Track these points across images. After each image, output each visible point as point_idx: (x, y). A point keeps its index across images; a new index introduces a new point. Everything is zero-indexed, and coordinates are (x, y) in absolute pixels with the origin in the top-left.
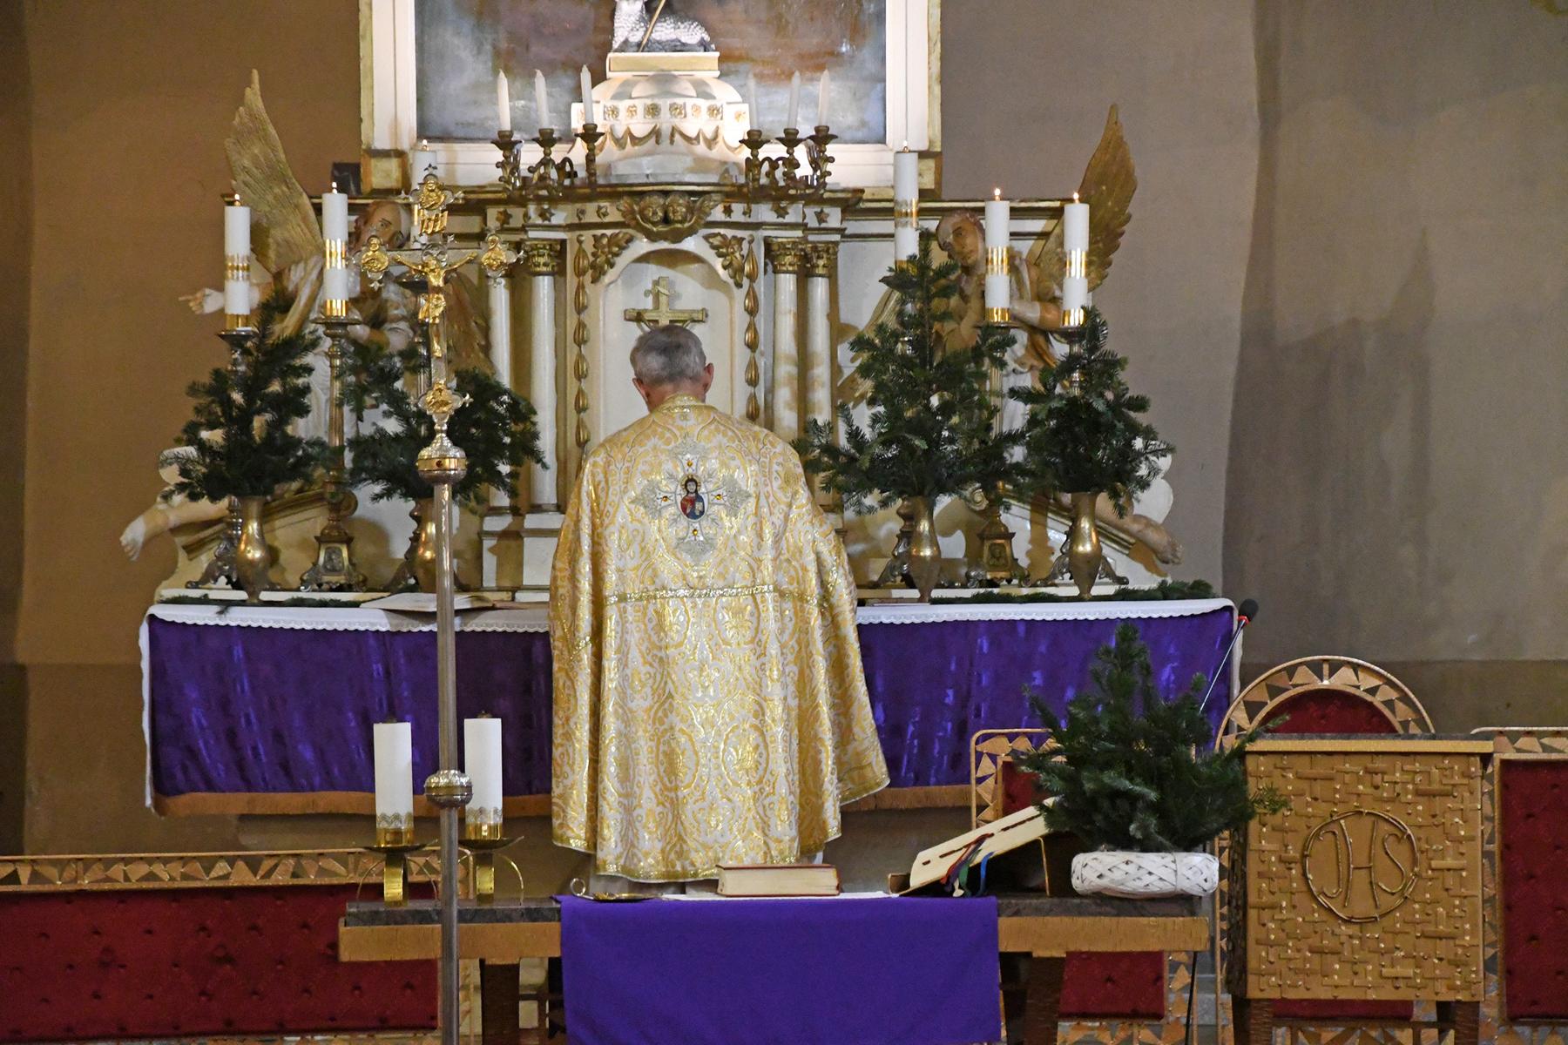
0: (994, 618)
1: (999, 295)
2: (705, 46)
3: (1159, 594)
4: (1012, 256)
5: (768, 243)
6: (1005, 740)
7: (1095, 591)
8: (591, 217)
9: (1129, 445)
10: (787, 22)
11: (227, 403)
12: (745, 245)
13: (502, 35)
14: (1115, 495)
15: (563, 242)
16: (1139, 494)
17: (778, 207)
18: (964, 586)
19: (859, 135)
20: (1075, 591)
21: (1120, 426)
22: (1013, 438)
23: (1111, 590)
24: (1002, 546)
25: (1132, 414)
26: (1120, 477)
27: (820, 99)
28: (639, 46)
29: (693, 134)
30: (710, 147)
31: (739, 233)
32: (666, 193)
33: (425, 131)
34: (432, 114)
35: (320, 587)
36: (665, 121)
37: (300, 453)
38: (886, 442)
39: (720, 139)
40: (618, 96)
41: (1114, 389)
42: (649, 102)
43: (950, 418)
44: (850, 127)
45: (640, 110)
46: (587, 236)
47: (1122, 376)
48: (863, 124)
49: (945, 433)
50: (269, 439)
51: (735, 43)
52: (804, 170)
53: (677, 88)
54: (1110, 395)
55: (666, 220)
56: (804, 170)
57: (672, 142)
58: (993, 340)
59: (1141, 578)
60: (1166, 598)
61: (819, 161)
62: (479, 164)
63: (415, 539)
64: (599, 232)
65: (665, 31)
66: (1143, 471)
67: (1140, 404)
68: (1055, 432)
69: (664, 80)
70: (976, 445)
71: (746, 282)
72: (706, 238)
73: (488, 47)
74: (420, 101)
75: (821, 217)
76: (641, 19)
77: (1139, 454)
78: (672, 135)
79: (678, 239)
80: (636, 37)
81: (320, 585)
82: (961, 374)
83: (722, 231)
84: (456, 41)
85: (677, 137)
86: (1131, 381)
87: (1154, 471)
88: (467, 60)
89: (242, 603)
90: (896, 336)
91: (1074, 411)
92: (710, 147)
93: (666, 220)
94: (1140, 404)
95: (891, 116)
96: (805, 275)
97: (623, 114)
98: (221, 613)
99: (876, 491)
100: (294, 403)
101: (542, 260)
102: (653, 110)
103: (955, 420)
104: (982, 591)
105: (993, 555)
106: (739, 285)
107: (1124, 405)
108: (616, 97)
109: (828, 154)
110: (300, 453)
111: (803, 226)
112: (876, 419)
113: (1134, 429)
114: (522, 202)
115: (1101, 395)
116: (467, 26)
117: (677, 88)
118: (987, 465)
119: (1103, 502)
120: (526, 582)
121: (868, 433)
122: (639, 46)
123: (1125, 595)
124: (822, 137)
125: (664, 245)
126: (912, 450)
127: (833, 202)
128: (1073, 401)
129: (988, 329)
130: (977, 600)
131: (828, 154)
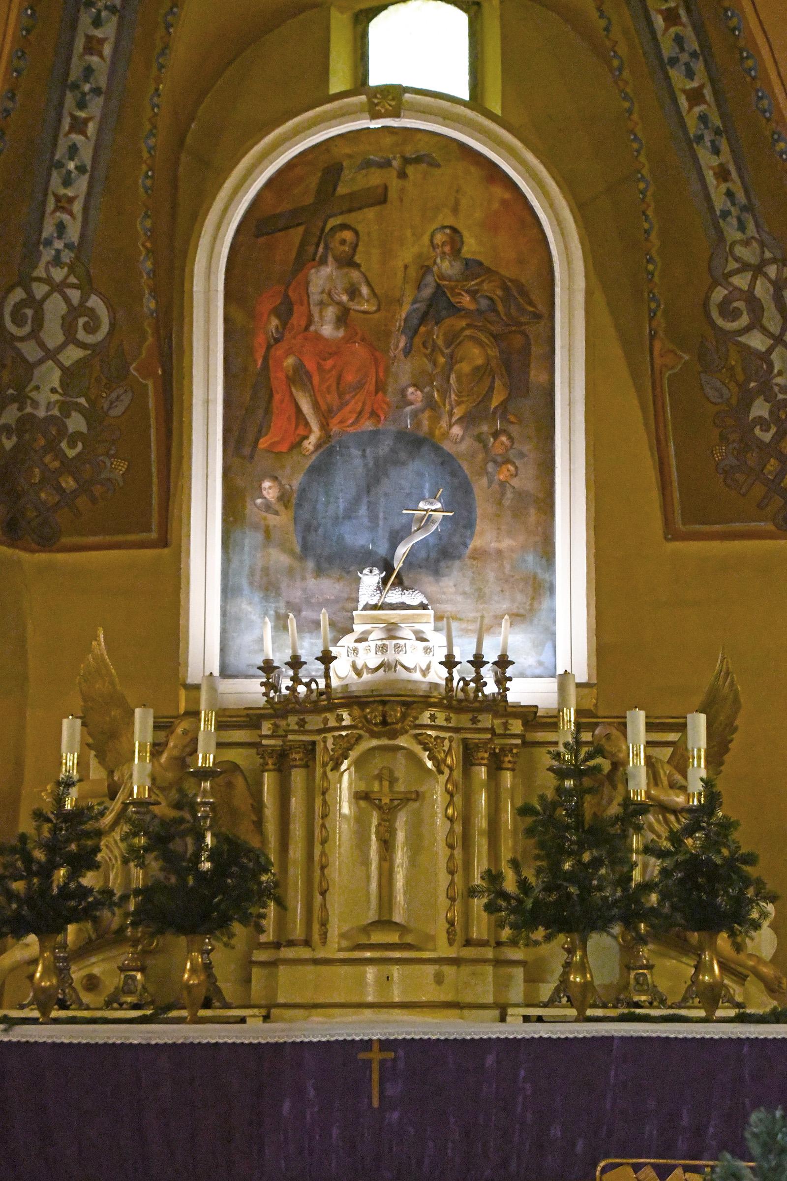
0: (635, 1034)
1: (639, 786)
2: (424, 607)
3: (773, 1018)
4: (650, 762)
5: (465, 742)
6: (630, 1170)
7: (720, 1013)
8: (332, 723)
9: (742, 892)
10: (485, 594)
11: (28, 859)
12: (447, 743)
13: (282, 604)
14: (733, 934)
15: (314, 743)
16: (753, 933)
17: (479, 721)
18: (615, 1007)
19: (538, 671)
20: (702, 1013)
21: (735, 877)
22: (647, 887)
23: (732, 1013)
24: (644, 975)
25: (744, 867)
26: (736, 919)
27: (517, 642)
28: (375, 607)
29: (411, 666)
30: (424, 675)
31: (442, 734)
32: (384, 703)
33: (225, 673)
34: (231, 659)
35: (121, 1006)
36: (391, 656)
37: (91, 899)
38: (548, 889)
39: (432, 670)
40: (359, 640)
41: (728, 847)
42: (379, 643)
43: (598, 870)
44: (530, 666)
45: (373, 649)
46: (329, 736)
47: (735, 835)
48: (540, 663)
49: (595, 882)
50: (63, 889)
51: (448, 608)
52: (491, 688)
53: (400, 634)
54: (725, 852)
55: (384, 723)
56: (491, 688)
57: (395, 671)
58: (633, 812)
59: (762, 1004)
60: (778, 1022)
61: (502, 681)
62: (251, 691)
63: (567, 965)
64: (337, 734)
65: (394, 596)
66: (755, 915)
67: (750, 859)
68: (681, 881)
69: (391, 632)
70: (619, 894)
71: (447, 771)
72: (416, 736)
73: (272, 612)
74: (223, 650)
75: (505, 725)
76: (378, 588)
77: (751, 901)
78: (396, 666)
79: (394, 735)
80: (373, 601)
81: (121, 1005)
82: (607, 838)
83: (429, 732)
84: (249, 609)
85: (399, 667)
86: (743, 839)
87: (764, 915)
88: (250, 607)
89: (34, 1021)
90: (554, 805)
91: (694, 867)
92: (424, 675)
93: (384, 723)
94: (750, 859)
95: (549, 655)
96: (496, 766)
97: (361, 652)
98: (6, 1030)
99: (541, 929)
100: (85, 860)
101: (297, 757)
102: (383, 649)
103: (603, 871)
104: (626, 1011)
105: (638, 983)
106: (441, 772)
107: (737, 860)
108: (359, 640)
109: (507, 675)
110: (91, 899)
111: (492, 730)
112: (539, 871)
113: (747, 881)
114: (284, 716)
115: (719, 852)
116: (257, 597)
117: (400, 634)
118: (630, 910)
119: (723, 940)
120: (281, 1000)
121: (532, 880)
122: (375, 607)
123: (742, 1019)
124: (503, 662)
125: (385, 742)
126: (569, 895)
127: (515, 715)
128: (694, 858)
129: (627, 801)
130: (622, 1019)
131: (507, 675)
